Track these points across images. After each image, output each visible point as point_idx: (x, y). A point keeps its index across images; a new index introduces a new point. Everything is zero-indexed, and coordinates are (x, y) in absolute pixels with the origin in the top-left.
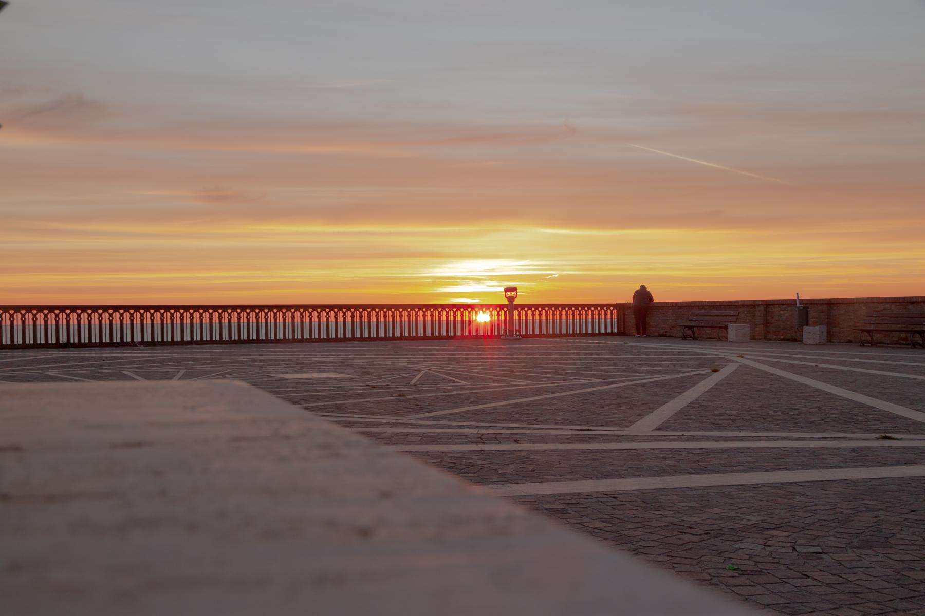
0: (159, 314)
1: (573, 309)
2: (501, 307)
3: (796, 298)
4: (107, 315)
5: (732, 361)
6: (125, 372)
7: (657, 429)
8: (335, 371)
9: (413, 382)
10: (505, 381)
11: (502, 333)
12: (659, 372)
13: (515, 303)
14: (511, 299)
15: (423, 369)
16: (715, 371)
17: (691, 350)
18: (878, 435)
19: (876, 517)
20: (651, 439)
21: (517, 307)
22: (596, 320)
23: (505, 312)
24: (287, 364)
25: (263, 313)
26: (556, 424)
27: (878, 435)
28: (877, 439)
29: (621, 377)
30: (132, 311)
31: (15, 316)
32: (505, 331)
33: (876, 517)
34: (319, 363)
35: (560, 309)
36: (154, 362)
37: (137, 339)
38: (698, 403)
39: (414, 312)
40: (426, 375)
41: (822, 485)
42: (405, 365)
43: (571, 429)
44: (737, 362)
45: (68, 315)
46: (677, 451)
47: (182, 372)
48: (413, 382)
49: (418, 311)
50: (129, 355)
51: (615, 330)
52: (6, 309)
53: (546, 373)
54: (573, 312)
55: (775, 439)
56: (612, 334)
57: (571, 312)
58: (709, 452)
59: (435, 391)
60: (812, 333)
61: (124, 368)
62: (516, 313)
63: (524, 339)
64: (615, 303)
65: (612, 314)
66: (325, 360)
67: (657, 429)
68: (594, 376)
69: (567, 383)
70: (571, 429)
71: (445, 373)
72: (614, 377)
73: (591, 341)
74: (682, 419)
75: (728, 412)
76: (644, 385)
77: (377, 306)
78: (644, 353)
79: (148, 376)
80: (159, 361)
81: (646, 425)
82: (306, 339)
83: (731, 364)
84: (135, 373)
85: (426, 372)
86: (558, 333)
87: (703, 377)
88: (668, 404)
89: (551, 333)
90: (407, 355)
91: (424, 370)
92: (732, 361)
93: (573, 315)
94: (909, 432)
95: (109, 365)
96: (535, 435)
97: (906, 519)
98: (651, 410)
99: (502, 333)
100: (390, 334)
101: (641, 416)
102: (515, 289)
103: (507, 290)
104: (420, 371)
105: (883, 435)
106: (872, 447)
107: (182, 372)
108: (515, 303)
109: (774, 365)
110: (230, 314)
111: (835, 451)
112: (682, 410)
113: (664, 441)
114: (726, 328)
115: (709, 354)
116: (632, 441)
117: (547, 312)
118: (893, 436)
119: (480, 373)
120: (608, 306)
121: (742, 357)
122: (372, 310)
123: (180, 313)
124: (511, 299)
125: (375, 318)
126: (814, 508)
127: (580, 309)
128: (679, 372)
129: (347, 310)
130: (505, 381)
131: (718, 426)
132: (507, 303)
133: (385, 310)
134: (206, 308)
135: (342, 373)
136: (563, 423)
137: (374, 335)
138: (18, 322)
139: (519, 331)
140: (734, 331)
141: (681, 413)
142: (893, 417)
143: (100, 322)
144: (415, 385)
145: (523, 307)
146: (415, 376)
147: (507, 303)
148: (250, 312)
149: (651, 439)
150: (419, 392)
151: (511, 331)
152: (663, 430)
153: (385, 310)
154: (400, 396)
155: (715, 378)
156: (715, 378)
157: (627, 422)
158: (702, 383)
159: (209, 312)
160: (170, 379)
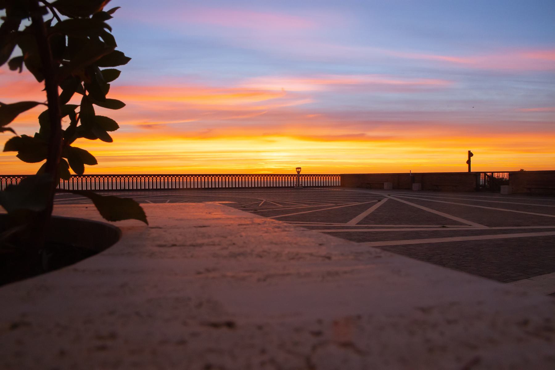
0: (189, 178)
1: (264, 176)
2: (295, 175)
3: (410, 172)
4: (143, 178)
5: (385, 197)
6: (146, 201)
7: (357, 224)
8: (229, 201)
9: (260, 205)
10: (297, 205)
11: (295, 185)
12: (358, 201)
13: (300, 174)
14: (299, 172)
15: (263, 200)
16: (379, 201)
17: (369, 193)
18: (441, 226)
19: (440, 257)
20: (355, 228)
21: (301, 175)
22: (309, 181)
23: (296, 177)
24: (209, 198)
25: (185, 177)
26: (317, 222)
27: (441, 226)
28: (440, 227)
29: (343, 203)
30: (153, 177)
31: (105, 178)
32: (296, 185)
33: (440, 257)
34: (222, 197)
35: (293, 176)
36: (157, 196)
37: (159, 187)
38: (372, 214)
39: (281, 177)
40: (265, 202)
41: (420, 245)
42: (257, 198)
43: (323, 224)
44: (387, 197)
45: (104, 178)
46: (366, 232)
47: (168, 201)
48: (260, 205)
49: (125, 178)
50: (148, 194)
51: (340, 185)
52: (4, 176)
53: (313, 202)
54: (304, 177)
55: (403, 228)
56: (339, 186)
57: (289, 177)
58: (377, 233)
59: (269, 209)
60: (416, 186)
61: (146, 199)
62: (300, 177)
63: (304, 188)
64: (340, 174)
65: (338, 178)
66: (224, 196)
67: (357, 224)
68: (332, 203)
69: (321, 206)
70: (323, 224)
71: (273, 202)
72: (340, 203)
73: (272, 191)
74: (366, 221)
75: (385, 217)
76: (352, 206)
77: (245, 175)
78: (351, 194)
79: (155, 202)
80: (159, 196)
81: (353, 222)
82: (135, 189)
83: (385, 198)
84: (150, 201)
85: (265, 201)
86: (287, 186)
87: (375, 203)
88: (361, 214)
89: (275, 186)
90: (257, 194)
91: (264, 200)
92: (385, 197)
93: (323, 178)
94: (452, 224)
95: (141, 198)
96: (310, 226)
97: (451, 258)
98: (355, 216)
99: (295, 185)
100: (159, 187)
101: (351, 219)
102: (300, 168)
103: (297, 168)
104: (262, 201)
105: (443, 226)
106: (439, 231)
107: (168, 201)
108: (300, 174)
109: (401, 199)
110: (187, 178)
111: (425, 232)
112: (367, 216)
113: (360, 229)
114: (383, 184)
115: (377, 194)
116: (348, 229)
117: (333, 177)
118: (446, 226)
119: (287, 202)
120: (337, 175)
121: (390, 196)
122: (209, 176)
123: (81, 178)
124: (299, 172)
125: (241, 180)
126: (418, 254)
127: (261, 176)
128: (366, 201)
129: (233, 176)
130: (297, 205)
131: (381, 223)
132: (297, 174)
133: (245, 176)
134: (224, 175)
135: (232, 201)
136: (320, 222)
137: (166, 187)
138: (89, 181)
139: (302, 185)
140: (386, 186)
141: (367, 217)
142: (446, 219)
143: (124, 181)
144: (261, 206)
145: (303, 175)
146: (260, 203)
147: (297, 174)
148: (125, 178)
149: (355, 228)
150: (263, 209)
151: (299, 185)
152: (360, 224)
153: (245, 176)
154: (255, 210)
155: (380, 204)
156: (380, 204)
157: (346, 221)
158: (374, 206)
159: (107, 177)
160: (165, 203)
